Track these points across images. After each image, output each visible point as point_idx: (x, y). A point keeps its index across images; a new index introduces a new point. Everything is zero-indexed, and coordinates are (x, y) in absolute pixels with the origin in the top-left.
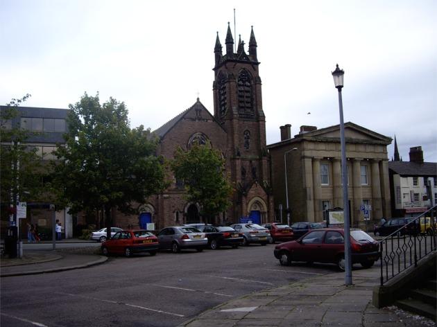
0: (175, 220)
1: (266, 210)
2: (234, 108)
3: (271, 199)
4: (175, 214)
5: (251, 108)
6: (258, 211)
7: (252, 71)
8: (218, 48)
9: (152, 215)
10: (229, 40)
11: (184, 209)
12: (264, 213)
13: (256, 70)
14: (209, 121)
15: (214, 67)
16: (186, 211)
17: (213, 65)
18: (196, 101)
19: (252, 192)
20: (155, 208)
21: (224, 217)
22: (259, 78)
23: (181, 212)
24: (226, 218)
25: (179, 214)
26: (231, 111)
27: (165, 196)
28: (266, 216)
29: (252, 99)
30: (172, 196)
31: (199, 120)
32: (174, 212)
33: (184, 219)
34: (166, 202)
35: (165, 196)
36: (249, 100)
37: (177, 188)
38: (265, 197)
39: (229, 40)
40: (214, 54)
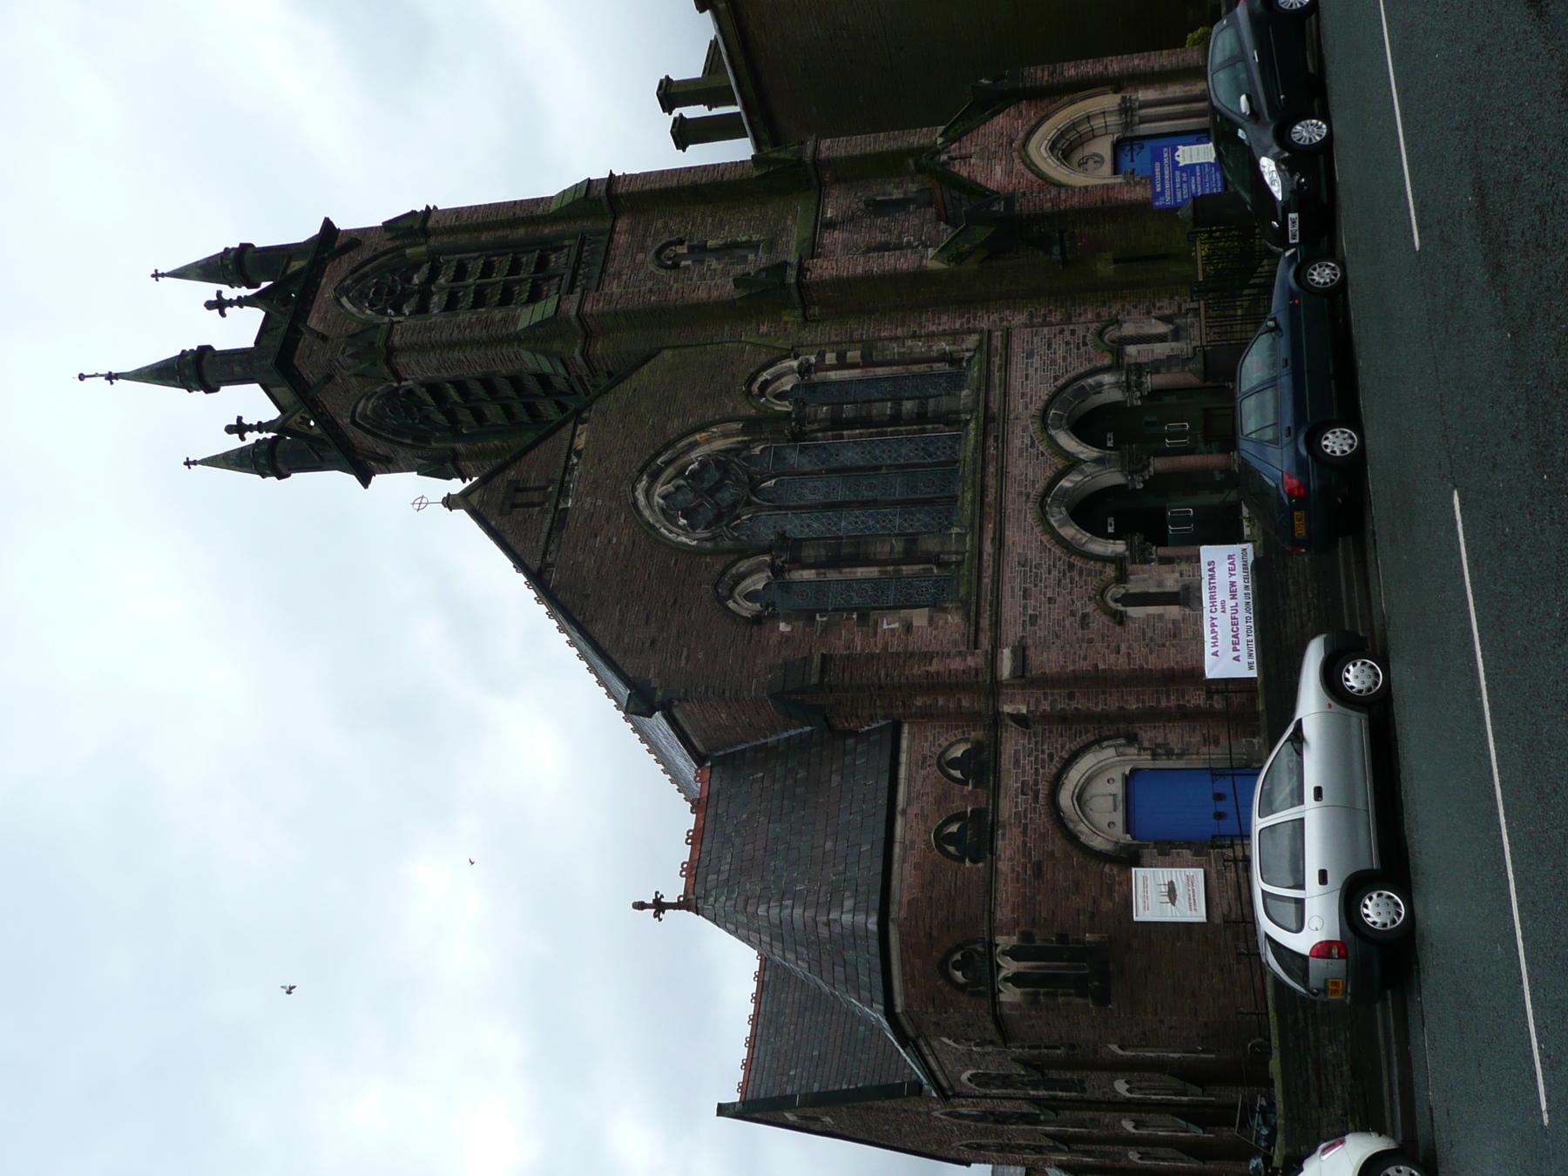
0: (1173, 611)
1: (1110, 101)
2: (528, 316)
3: (1041, 75)
4: (1134, 612)
5: (549, 246)
6: (1117, 147)
7: (358, 256)
8: (268, 457)
9: (1145, 761)
10: (197, 370)
11: (1104, 559)
12: (1126, 109)
13: (357, 239)
14: (580, 442)
15: (351, 480)
16: (1119, 547)
17: (340, 482)
18: (461, 515)
19: (996, 177)
20: (1098, 742)
21: (1161, 338)
22: (389, 225)
23: (1122, 578)
24: (1162, 328)
25: (1134, 587)
26: (537, 336)
27: (1006, 668)
28: (1144, 95)
29: (501, 247)
30: (1011, 632)
31: (563, 492)
32: (1120, 619)
33: (1166, 561)
34: (1047, 661)
35: (1006, 668)
36: (503, 263)
37: (964, 605)
38: (1029, 112)
39: (197, 370)
40: (297, 478)
